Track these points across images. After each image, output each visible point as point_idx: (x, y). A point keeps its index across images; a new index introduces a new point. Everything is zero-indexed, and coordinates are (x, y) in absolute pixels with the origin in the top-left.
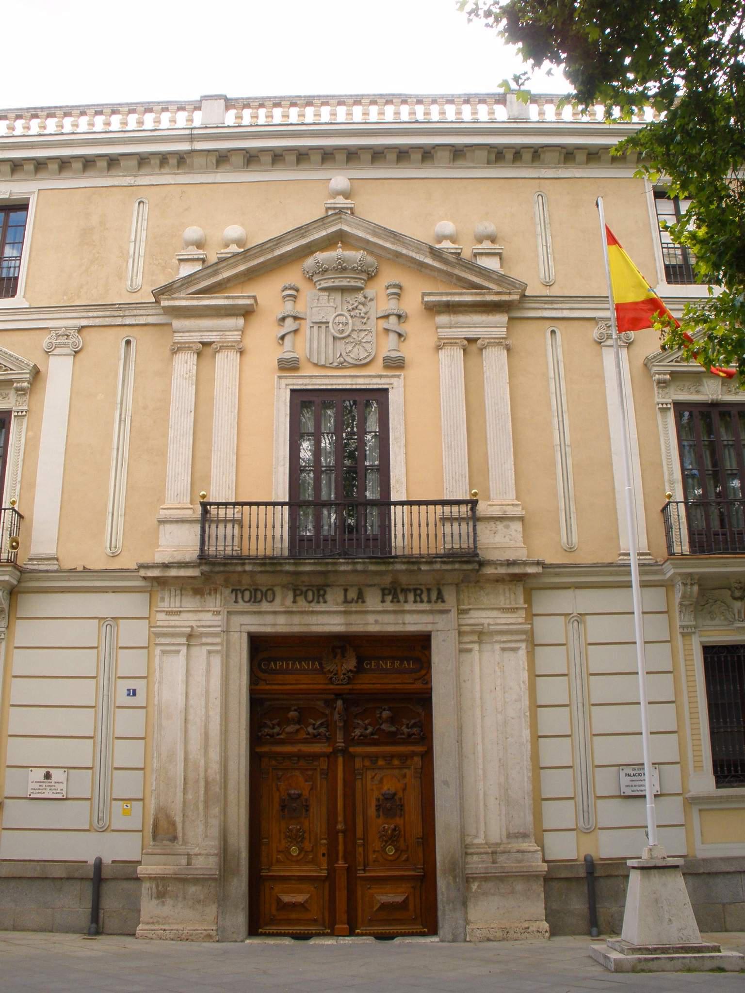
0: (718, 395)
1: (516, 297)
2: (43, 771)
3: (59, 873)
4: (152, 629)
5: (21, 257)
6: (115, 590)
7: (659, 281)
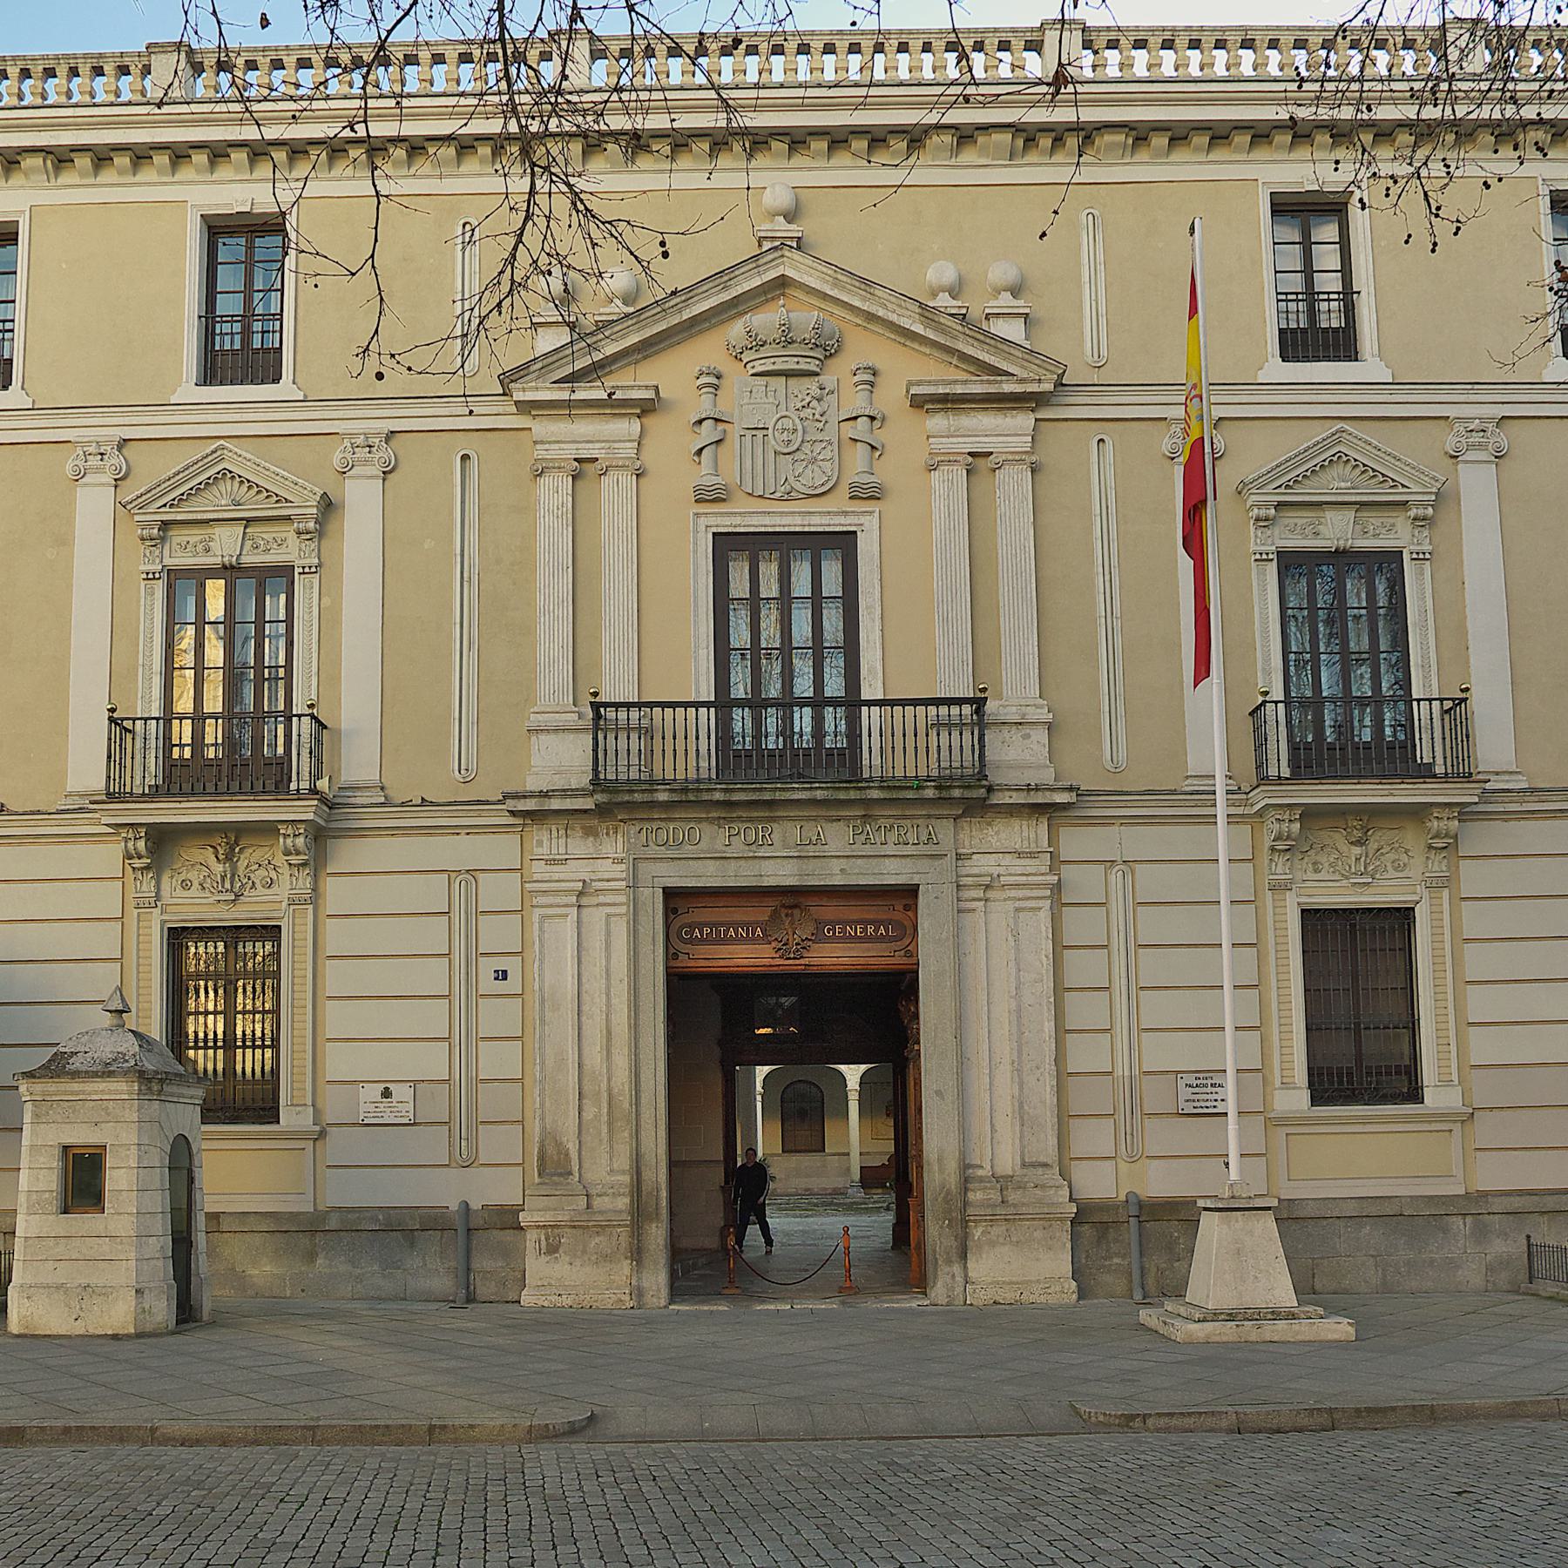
0: (1347, 540)
1: (1049, 387)
4: (527, 885)
5: (282, 315)
7: (1270, 356)
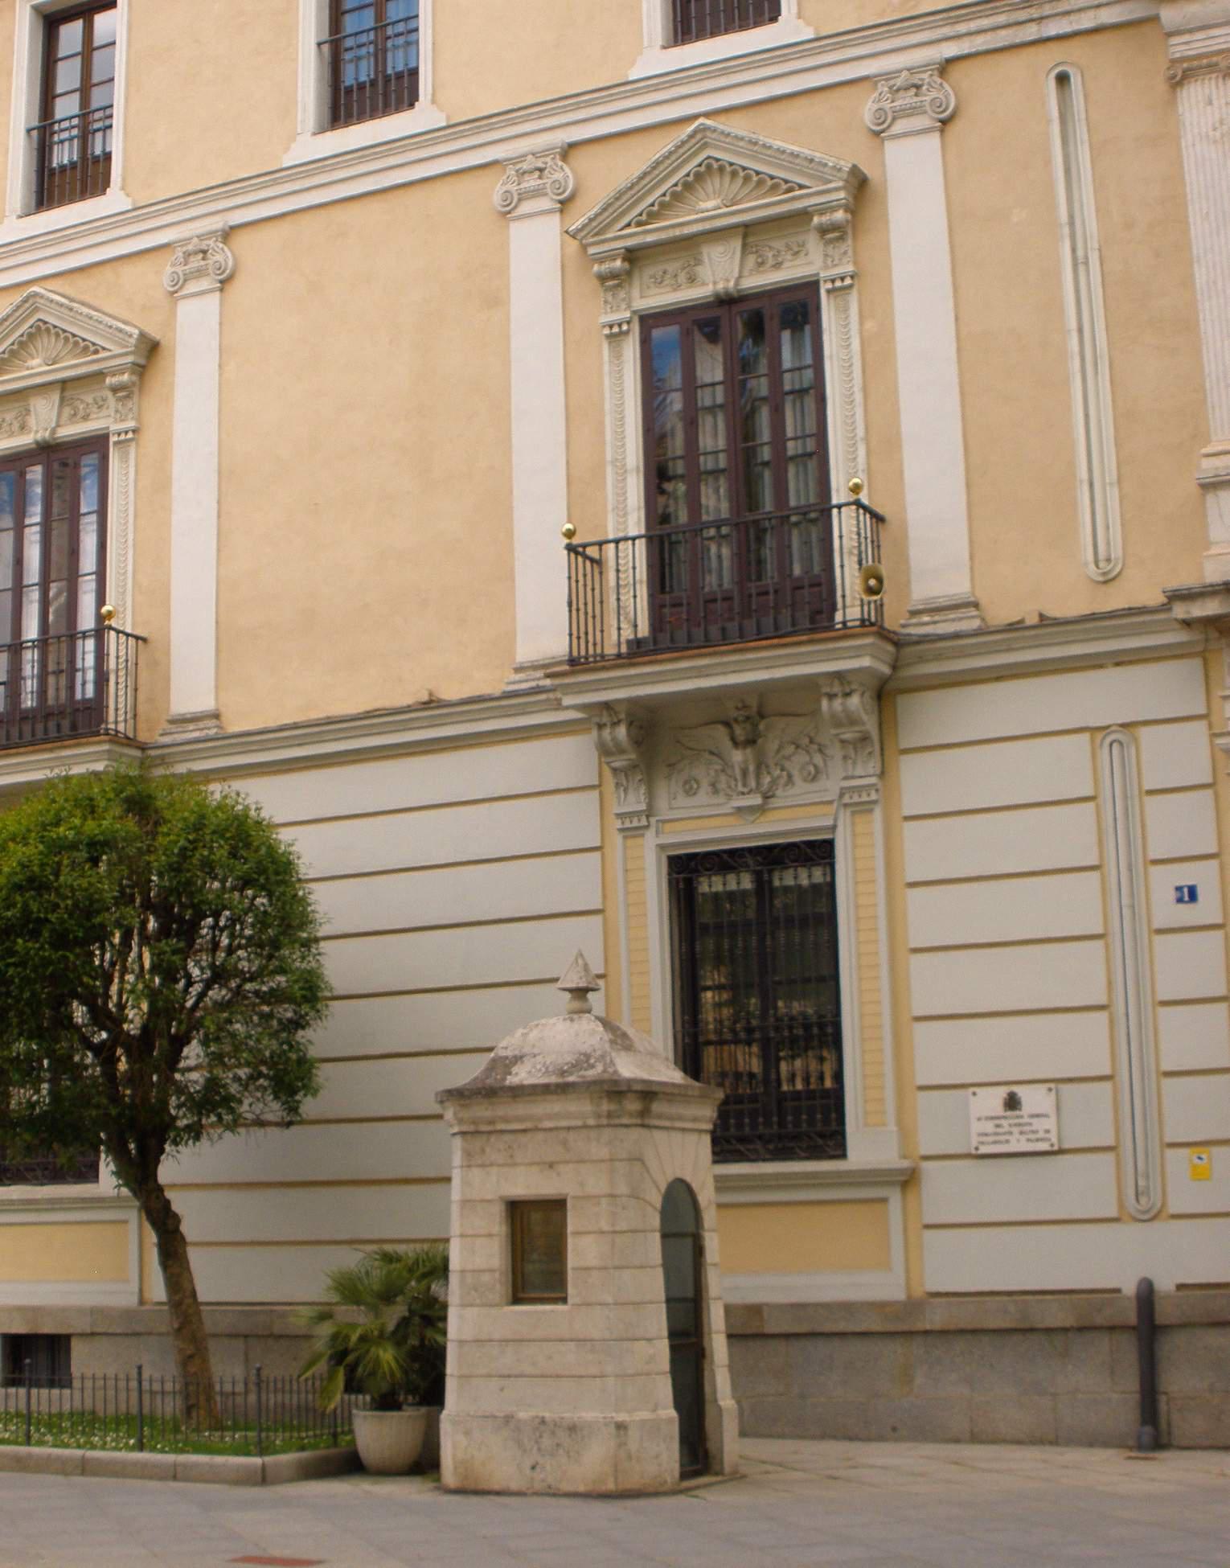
2: (1002, 1092)
3: (1057, 1316)
4: (1220, 741)
6: (1121, 659)
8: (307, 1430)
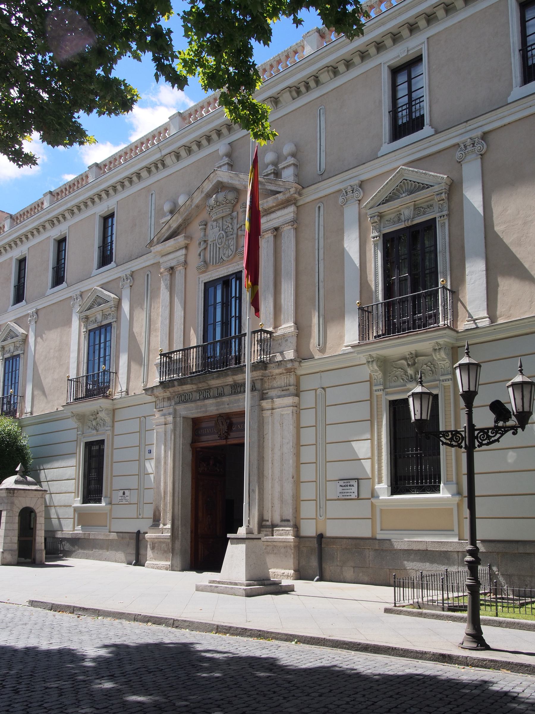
8: (458, 591)
